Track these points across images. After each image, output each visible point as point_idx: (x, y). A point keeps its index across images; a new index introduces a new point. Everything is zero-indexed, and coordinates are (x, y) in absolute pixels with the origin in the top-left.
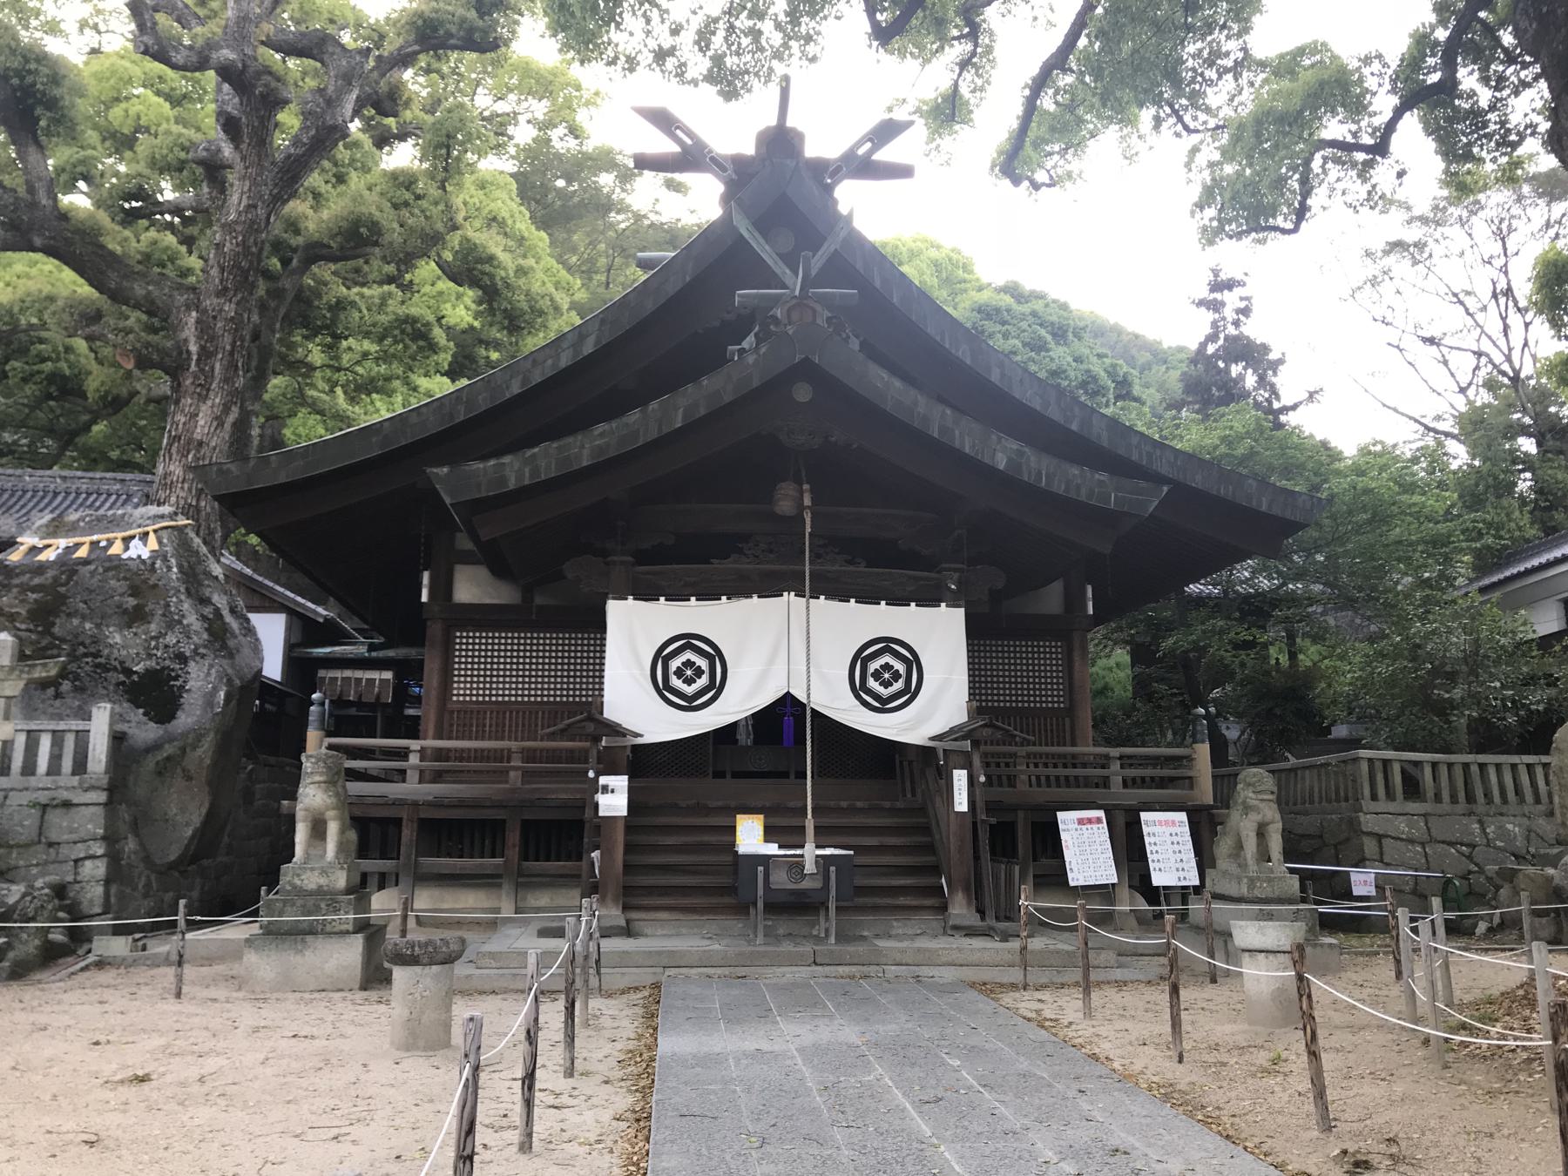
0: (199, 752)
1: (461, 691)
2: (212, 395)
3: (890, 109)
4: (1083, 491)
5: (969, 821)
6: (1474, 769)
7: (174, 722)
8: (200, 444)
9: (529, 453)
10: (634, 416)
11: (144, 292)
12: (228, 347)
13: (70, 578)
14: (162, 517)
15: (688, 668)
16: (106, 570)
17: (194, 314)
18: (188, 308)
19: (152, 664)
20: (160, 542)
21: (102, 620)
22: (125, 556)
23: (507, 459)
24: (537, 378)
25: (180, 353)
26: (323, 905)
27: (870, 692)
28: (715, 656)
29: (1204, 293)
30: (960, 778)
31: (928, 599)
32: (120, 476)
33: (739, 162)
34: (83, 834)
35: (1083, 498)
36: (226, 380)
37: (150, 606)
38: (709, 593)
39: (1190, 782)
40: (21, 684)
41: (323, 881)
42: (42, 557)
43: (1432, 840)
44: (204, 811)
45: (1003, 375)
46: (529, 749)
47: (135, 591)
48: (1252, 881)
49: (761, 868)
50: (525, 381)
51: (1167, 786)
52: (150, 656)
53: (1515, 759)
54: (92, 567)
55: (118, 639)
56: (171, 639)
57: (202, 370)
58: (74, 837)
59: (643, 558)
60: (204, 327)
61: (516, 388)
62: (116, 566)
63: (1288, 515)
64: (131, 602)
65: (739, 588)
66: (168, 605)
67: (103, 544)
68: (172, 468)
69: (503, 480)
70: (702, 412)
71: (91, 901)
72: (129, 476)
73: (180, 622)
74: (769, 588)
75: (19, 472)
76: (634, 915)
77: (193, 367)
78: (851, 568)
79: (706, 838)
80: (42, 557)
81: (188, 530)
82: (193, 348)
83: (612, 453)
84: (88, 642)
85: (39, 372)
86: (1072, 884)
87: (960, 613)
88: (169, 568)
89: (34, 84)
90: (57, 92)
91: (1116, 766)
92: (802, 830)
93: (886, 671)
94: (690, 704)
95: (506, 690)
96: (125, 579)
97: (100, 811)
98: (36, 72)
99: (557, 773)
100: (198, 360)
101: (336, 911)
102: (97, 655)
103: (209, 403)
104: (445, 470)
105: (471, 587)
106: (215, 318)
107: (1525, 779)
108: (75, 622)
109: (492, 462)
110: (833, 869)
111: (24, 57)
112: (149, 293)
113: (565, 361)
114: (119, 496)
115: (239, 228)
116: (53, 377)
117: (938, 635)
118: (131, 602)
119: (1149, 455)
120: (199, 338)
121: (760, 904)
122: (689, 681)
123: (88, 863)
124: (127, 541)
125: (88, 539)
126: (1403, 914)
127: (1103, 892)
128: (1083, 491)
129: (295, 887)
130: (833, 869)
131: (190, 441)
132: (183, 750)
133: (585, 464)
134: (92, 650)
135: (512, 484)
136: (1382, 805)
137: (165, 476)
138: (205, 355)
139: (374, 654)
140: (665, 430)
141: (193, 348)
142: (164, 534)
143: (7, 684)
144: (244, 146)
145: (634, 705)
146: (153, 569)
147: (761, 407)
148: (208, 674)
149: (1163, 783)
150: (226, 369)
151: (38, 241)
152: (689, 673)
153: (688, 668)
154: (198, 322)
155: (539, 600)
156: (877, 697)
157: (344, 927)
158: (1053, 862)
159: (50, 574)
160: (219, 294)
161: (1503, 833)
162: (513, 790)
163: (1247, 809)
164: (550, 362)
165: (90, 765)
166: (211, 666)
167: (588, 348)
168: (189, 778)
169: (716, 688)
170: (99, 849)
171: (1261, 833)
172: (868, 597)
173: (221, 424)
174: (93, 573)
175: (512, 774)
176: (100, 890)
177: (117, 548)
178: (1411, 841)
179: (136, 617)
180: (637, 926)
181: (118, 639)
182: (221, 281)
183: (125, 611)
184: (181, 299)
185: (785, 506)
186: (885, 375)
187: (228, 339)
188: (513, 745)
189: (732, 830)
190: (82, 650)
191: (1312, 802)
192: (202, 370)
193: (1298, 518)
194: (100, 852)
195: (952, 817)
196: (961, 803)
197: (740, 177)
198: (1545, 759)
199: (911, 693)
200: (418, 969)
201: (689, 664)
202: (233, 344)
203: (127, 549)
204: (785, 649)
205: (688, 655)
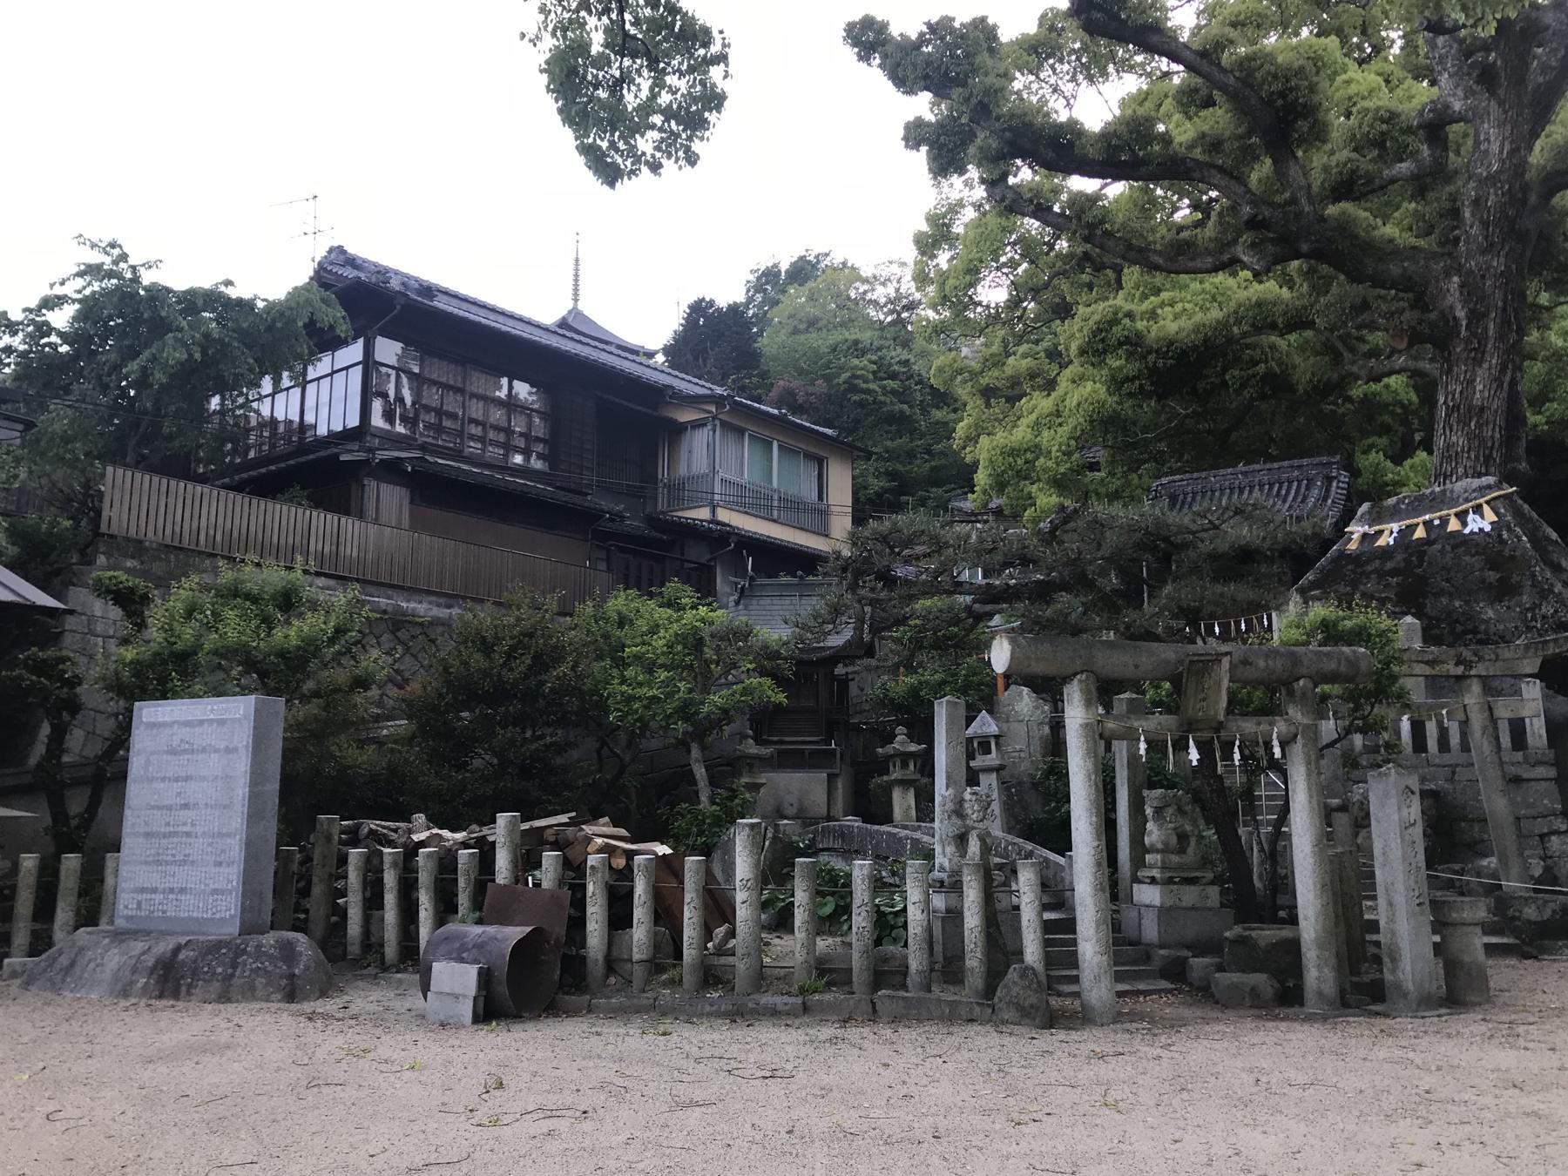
3: (52, 286)
8: (1482, 409)
11: (1400, 271)
13: (1421, 561)
14: (1489, 487)
16: (1454, 547)
17: (1456, 279)
20: (1497, 513)
22: (1467, 531)
32: (1296, 462)
36: (1501, 338)
37: (1515, 578)
40: (1539, 661)
42: (1381, 542)
52: (1529, 629)
54: (1438, 546)
55: (1491, 614)
56: (1547, 609)
57: (1474, 334)
60: (1471, 290)
62: (1461, 541)
66: (1533, 575)
67: (1437, 522)
68: (1454, 439)
72: (1305, 462)
73: (1551, 591)
75: (1204, 474)
80: (1381, 542)
81: (1515, 497)
82: (1460, 313)
84: (1462, 619)
85: (1254, 376)
88: (1519, 539)
89: (1297, 99)
90: (1316, 99)
96: (1477, 553)
98: (1297, 88)
102: (1475, 631)
103: (1486, 366)
106: (1483, 277)
108: (1444, 601)
111: (1285, 77)
112: (1405, 269)
114: (1300, 482)
116: (1269, 377)
118: (1492, 576)
120: (1465, 303)
124: (1462, 516)
125: (1420, 520)
131: (1470, 408)
134: (1470, 627)
137: (1448, 447)
138: (1475, 317)
141: (1460, 313)
142: (1499, 504)
143: (1526, 662)
144: (1501, 92)
146: (1502, 541)
151: (1305, 248)
154: (1462, 286)
159: (1399, 557)
160: (1484, 252)
165: (1530, 740)
173: (1500, 386)
174: (1442, 551)
177: (1454, 525)
179: (1503, 591)
181: (1491, 614)
187: (1499, 295)
190: (1459, 628)
192: (1474, 334)
202: (1505, 301)
203: (1465, 524)
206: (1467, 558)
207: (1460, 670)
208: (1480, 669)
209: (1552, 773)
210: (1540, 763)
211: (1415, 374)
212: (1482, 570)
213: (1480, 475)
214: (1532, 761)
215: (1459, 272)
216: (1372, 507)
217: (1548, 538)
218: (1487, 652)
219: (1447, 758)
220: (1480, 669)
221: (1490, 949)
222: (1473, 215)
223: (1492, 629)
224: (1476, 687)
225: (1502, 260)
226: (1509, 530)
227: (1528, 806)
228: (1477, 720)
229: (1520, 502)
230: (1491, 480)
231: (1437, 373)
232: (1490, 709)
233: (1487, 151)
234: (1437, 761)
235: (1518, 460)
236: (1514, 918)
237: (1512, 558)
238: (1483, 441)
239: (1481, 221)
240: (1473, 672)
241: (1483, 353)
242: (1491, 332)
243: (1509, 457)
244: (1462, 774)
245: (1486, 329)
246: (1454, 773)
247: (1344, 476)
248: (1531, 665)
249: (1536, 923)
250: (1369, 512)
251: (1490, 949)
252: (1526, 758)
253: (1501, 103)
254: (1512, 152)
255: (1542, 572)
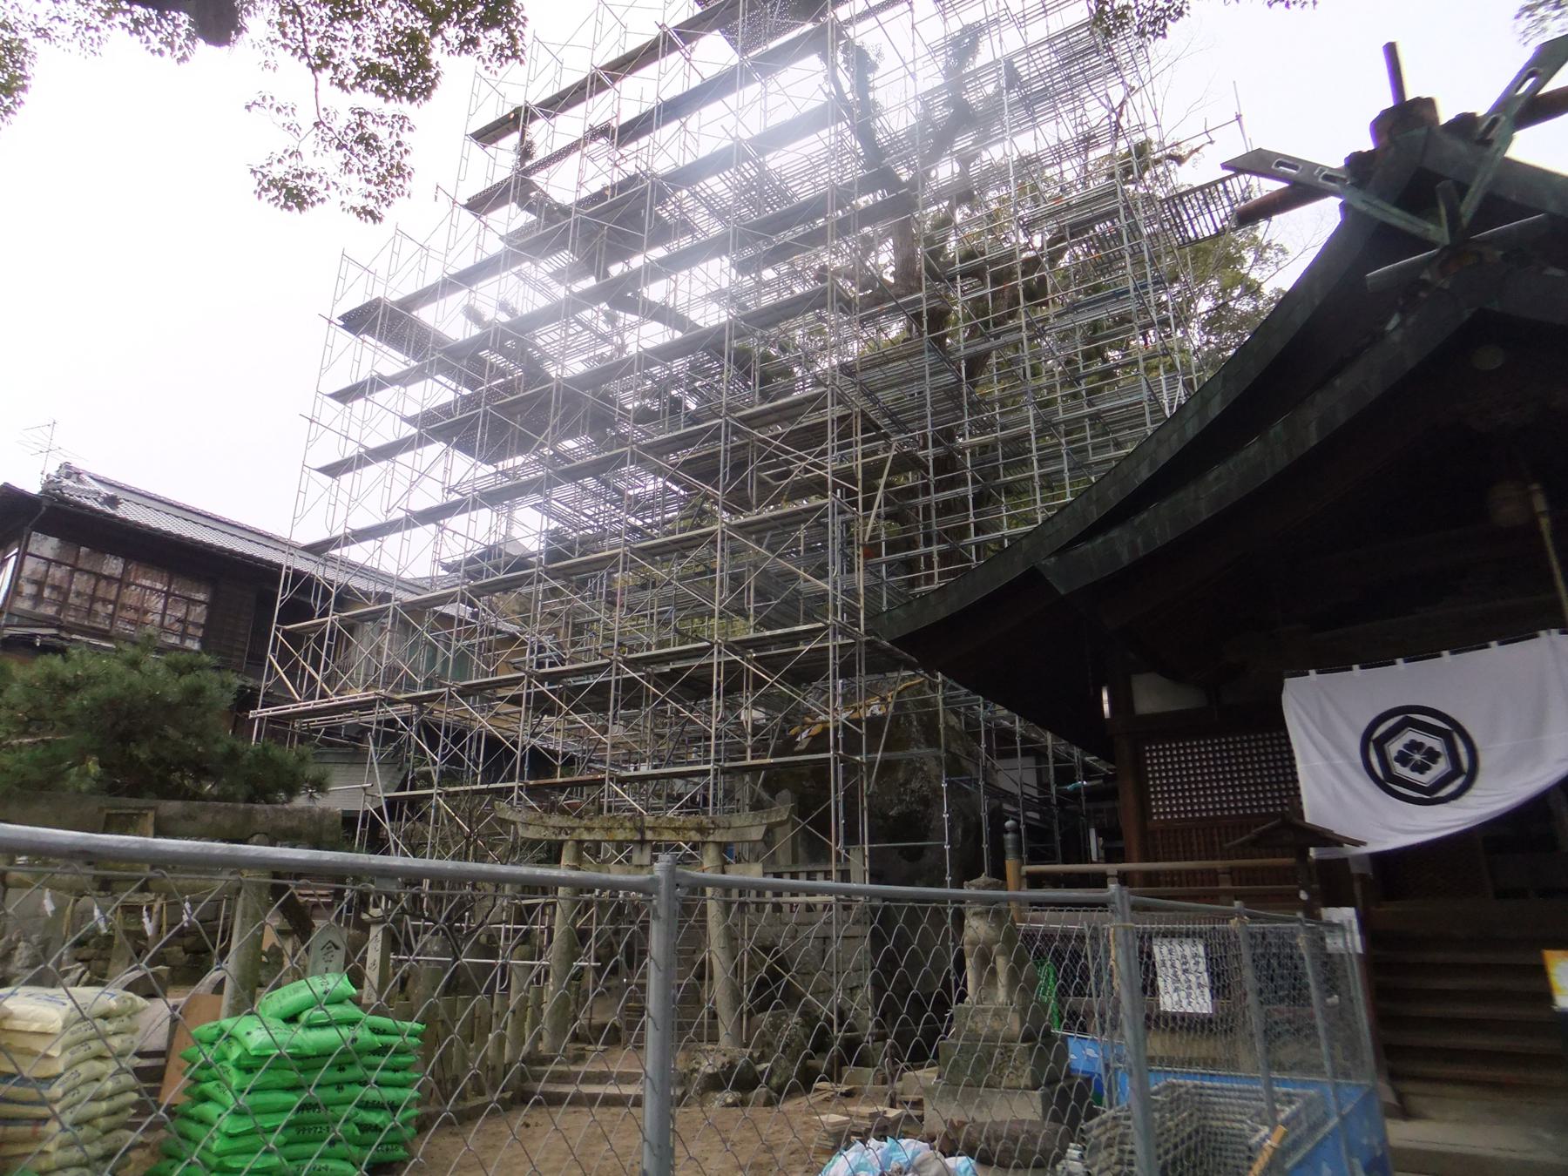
1: (1162, 809)
9: (1137, 521)
10: (1254, 448)
15: (1419, 752)
19: (902, 808)
23: (1115, 533)
24: (1164, 456)
28: (1452, 731)
33: (1357, 162)
38: (1421, 649)
46: (1240, 869)
52: (901, 801)
61: (1145, 473)
73: (921, 769)
76: (1408, 1087)
79: (1450, 984)
94: (1429, 796)
105: (1151, 698)
109: (1100, 540)
122: (1421, 768)
133: (1204, 517)
135: (1126, 558)
145: (1342, 799)
164: (1175, 436)
167: (1215, 410)
180: (1416, 1103)
188: (1218, 864)
189: (1541, 972)
201: (1414, 746)
205: (1410, 735)
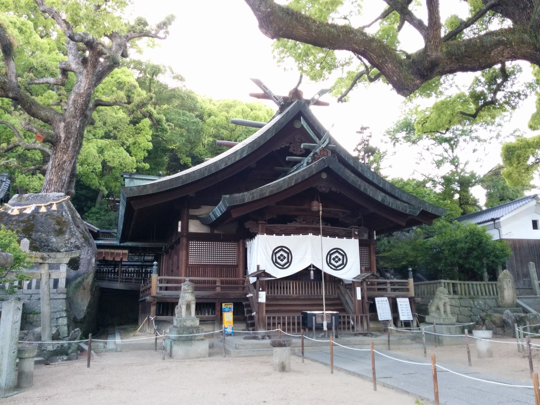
0: (88, 280)
2: (68, 152)
4: (401, 208)
5: (361, 302)
6: (470, 285)
7: (79, 270)
12: (76, 136)
15: (282, 256)
18: (60, 121)
21: (48, 233)
25: (57, 137)
26: (195, 331)
27: (332, 264)
28: (289, 253)
29: (359, 130)
30: (358, 290)
31: (349, 236)
34: (59, 309)
35: (400, 210)
38: (288, 233)
39: (408, 290)
41: (192, 323)
43: (461, 306)
44: (89, 300)
45: (362, 169)
47: (58, 223)
48: (444, 319)
49: (314, 317)
50: (226, 164)
51: (403, 290)
52: (66, 246)
53: (448, 281)
56: (73, 240)
57: (65, 144)
58: (55, 310)
59: (271, 221)
63: (436, 214)
64: (57, 227)
65: (297, 232)
69: (244, 199)
70: (300, 181)
71: (63, 332)
73: (75, 234)
74: (305, 231)
77: (62, 142)
78: (327, 227)
83: (275, 192)
84: (44, 241)
86: (380, 319)
87: (357, 241)
88: (68, 215)
91: (389, 285)
92: (322, 305)
93: (337, 257)
94: (283, 267)
95: (205, 261)
96: (54, 219)
97: (64, 301)
99: (231, 288)
100: (64, 140)
101: (199, 333)
102: (48, 246)
104: (228, 196)
107: (479, 287)
109: (242, 194)
110: (334, 317)
113: (238, 158)
115: (84, 95)
117: (351, 247)
118: (57, 227)
119: (401, 195)
121: (314, 328)
123: (60, 319)
126: (516, 325)
127: (386, 322)
128: (401, 208)
129: (184, 325)
130: (334, 317)
132: (83, 280)
133: (267, 195)
134: (46, 244)
135: (246, 201)
136: (485, 296)
138: (67, 138)
139: (122, 244)
140: (290, 186)
143: (64, 259)
144: (88, 68)
147: (291, 175)
148: (88, 253)
149: (402, 290)
150: (74, 144)
151: (11, 95)
152: (282, 258)
153: (282, 256)
154: (65, 127)
155: (216, 232)
156: (334, 266)
157: (201, 338)
158: (374, 314)
161: (479, 304)
162: (218, 294)
163: (441, 299)
164: (233, 158)
166: (88, 250)
167: (244, 155)
168: (84, 289)
169: (289, 262)
170: (64, 314)
171: (445, 305)
172: (333, 235)
175: (217, 288)
176: (66, 328)
178: (456, 306)
179: (60, 232)
181: (54, 240)
182: (75, 113)
183: (56, 230)
184: (57, 118)
185: (315, 208)
186: (350, 172)
191: (424, 295)
192: (65, 144)
193: (439, 214)
194: (65, 315)
195: (357, 301)
196: (359, 297)
197: (284, 104)
198: (495, 282)
199: (344, 265)
200: (284, 348)
204: (308, 250)
205: (282, 253)
206: (50, 220)
207: (41, 261)
208: (49, 261)
209: (64, 296)
210: (62, 293)
211: (43, 152)
212: (54, 225)
213: (59, 191)
214: (59, 292)
215: (64, 121)
216: (19, 196)
217: (77, 217)
218: (52, 254)
219: (30, 291)
220: (49, 261)
221: (37, 363)
222: (72, 104)
223: (54, 245)
224: (46, 267)
225: (79, 122)
226: (66, 212)
227: (55, 308)
228: (44, 279)
229: (70, 203)
230: (62, 194)
231: (50, 153)
232: (50, 275)
233: (80, 85)
234: (26, 292)
235: (72, 189)
236: (44, 350)
237: (65, 222)
238: (62, 180)
239: (74, 107)
240: (47, 262)
241: (67, 150)
242: (71, 144)
243: (69, 187)
244: (35, 297)
245: (69, 143)
246: (31, 297)
247: (8, 182)
248: (67, 260)
249: (51, 351)
250: (17, 198)
251: (37, 363)
252: (57, 291)
253: (87, 71)
254: (89, 88)
255: (73, 228)
